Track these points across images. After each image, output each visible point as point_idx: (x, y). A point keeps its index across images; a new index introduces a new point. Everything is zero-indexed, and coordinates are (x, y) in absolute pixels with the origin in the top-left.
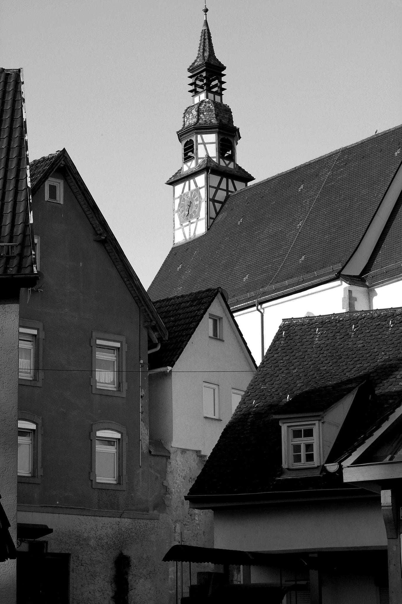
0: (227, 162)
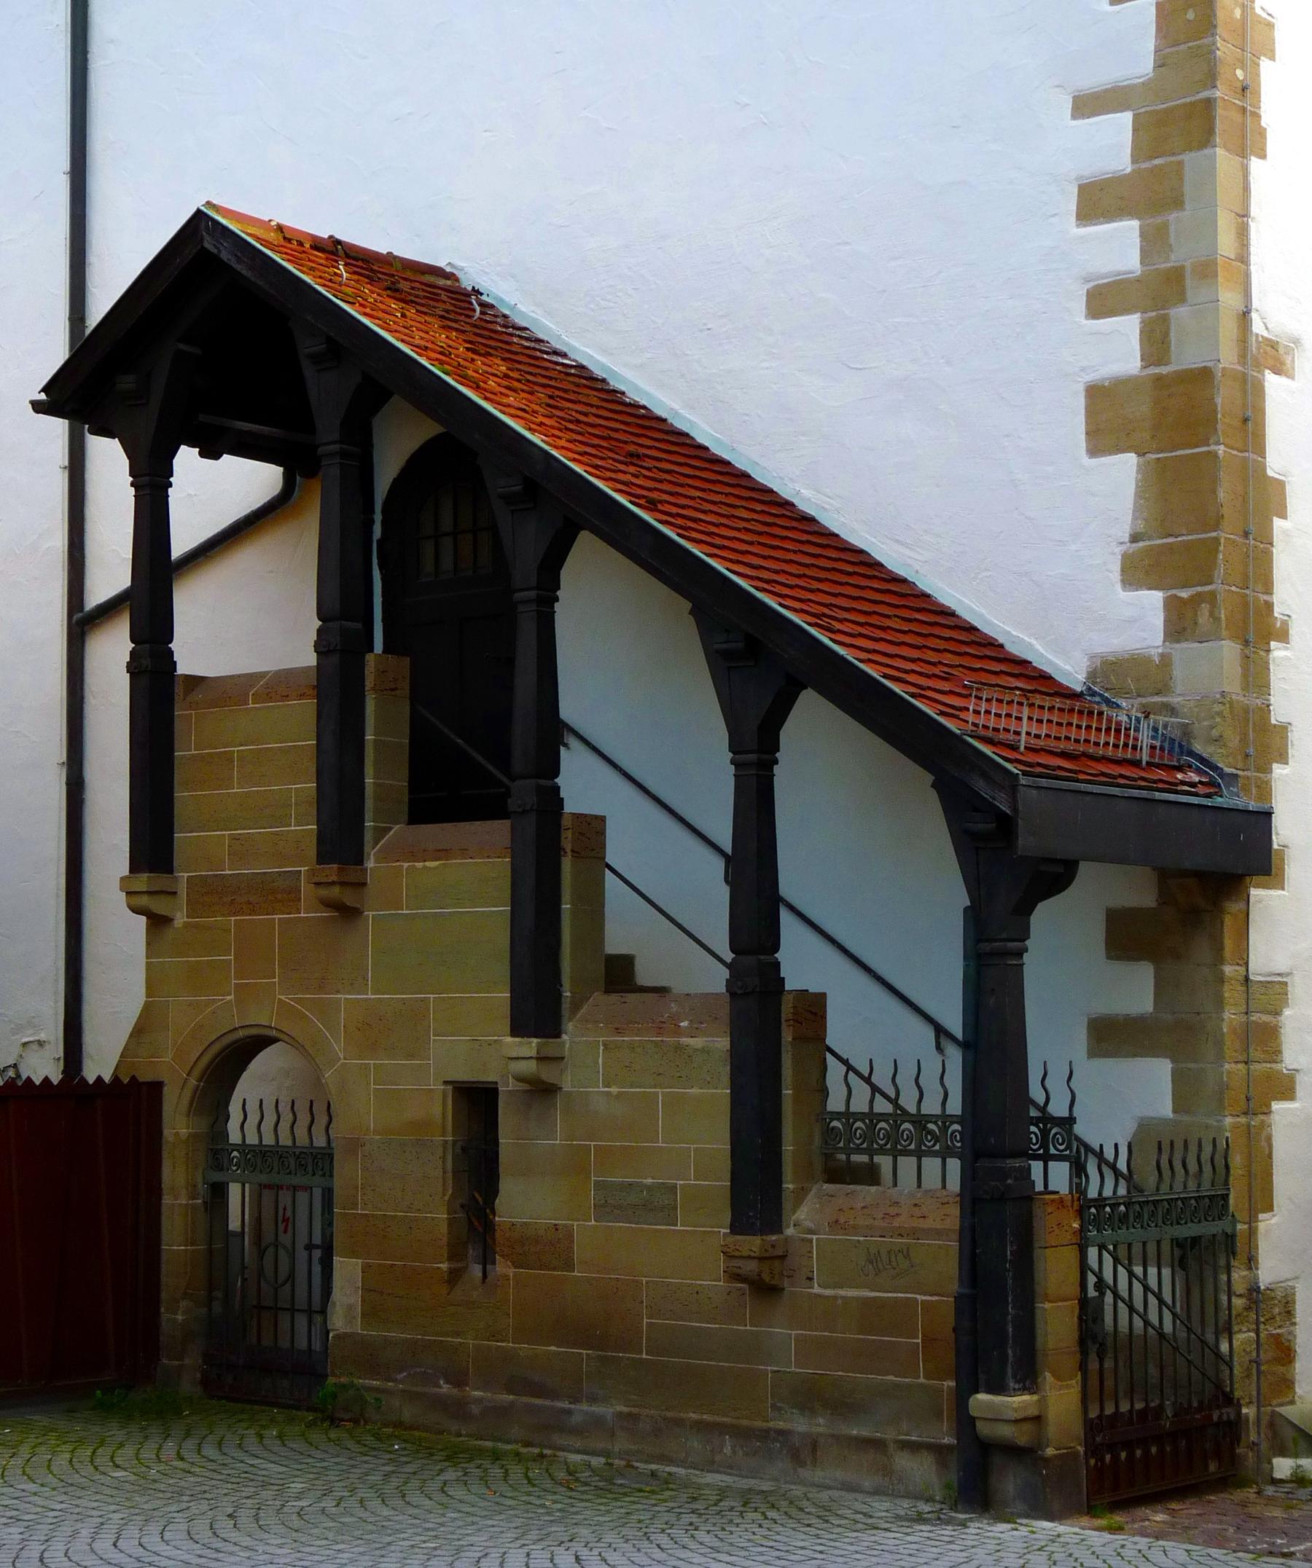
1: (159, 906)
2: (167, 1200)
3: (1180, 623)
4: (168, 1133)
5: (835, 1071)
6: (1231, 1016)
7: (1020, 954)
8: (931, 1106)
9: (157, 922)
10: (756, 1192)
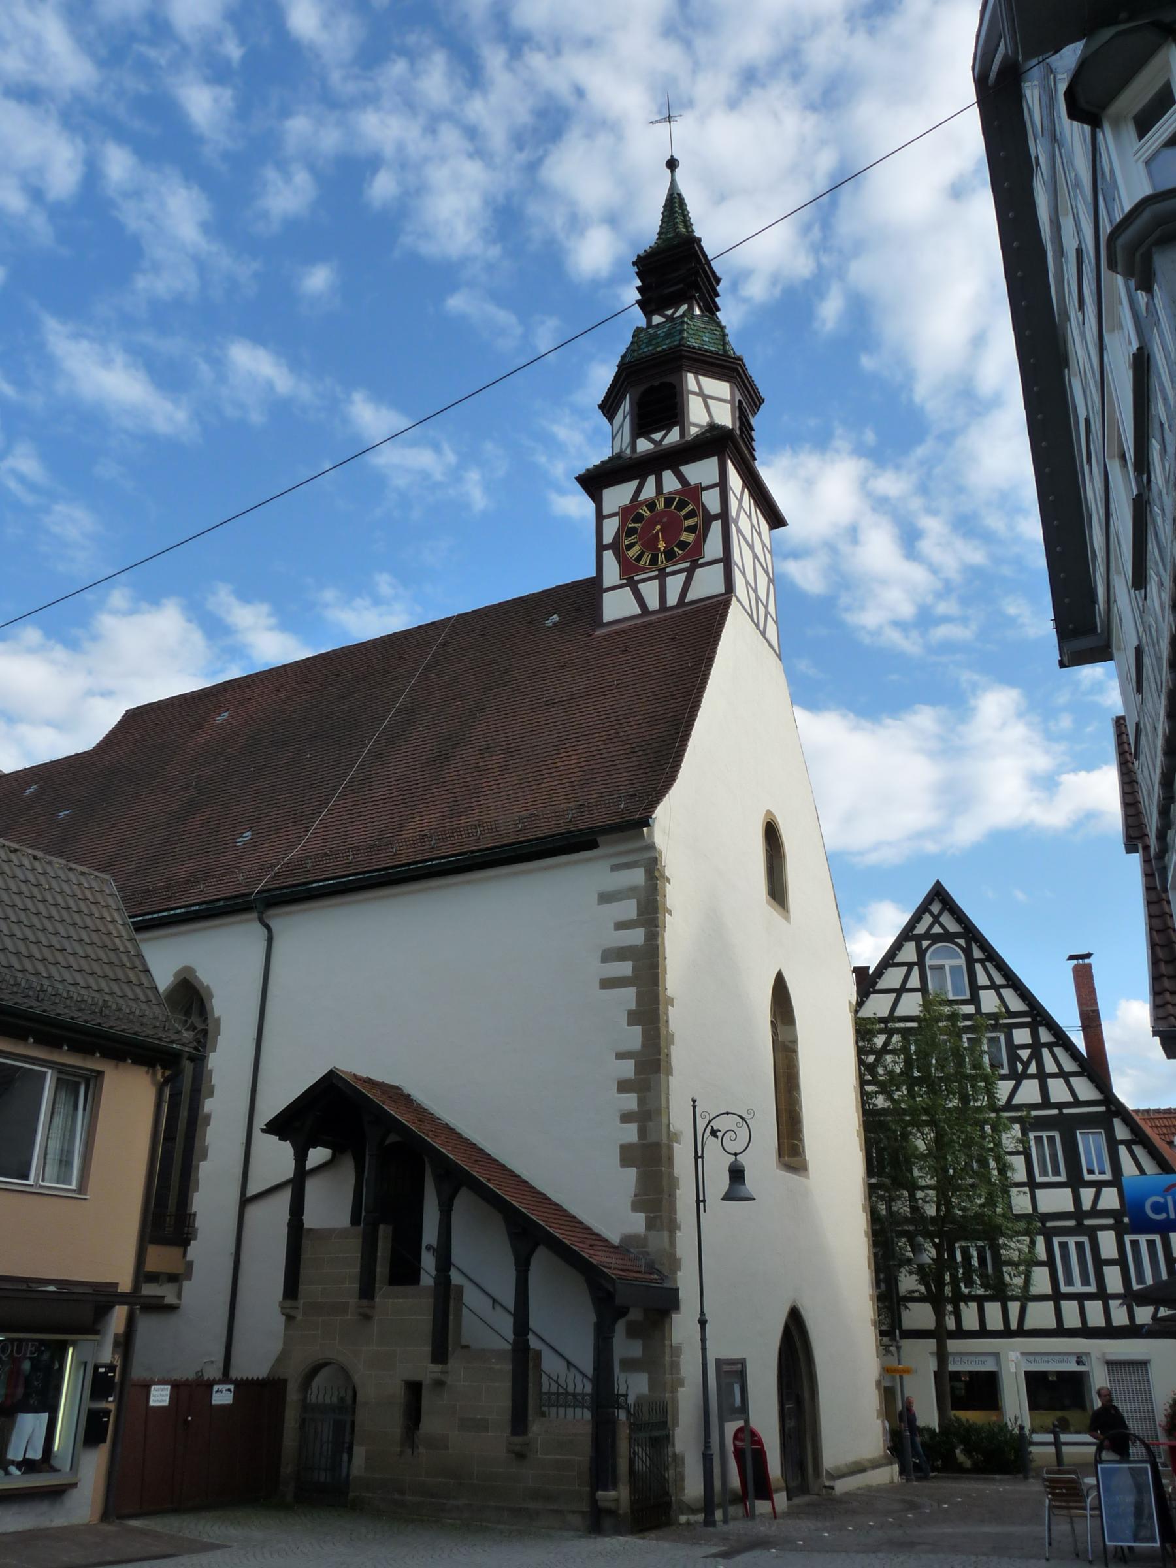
0: (657, 436)
1: (293, 1312)
2: (286, 1425)
3: (650, 1225)
4: (288, 1399)
5: (545, 1379)
6: (667, 1358)
7: (612, 1338)
8: (579, 1390)
9: (289, 1318)
10: (519, 1422)
